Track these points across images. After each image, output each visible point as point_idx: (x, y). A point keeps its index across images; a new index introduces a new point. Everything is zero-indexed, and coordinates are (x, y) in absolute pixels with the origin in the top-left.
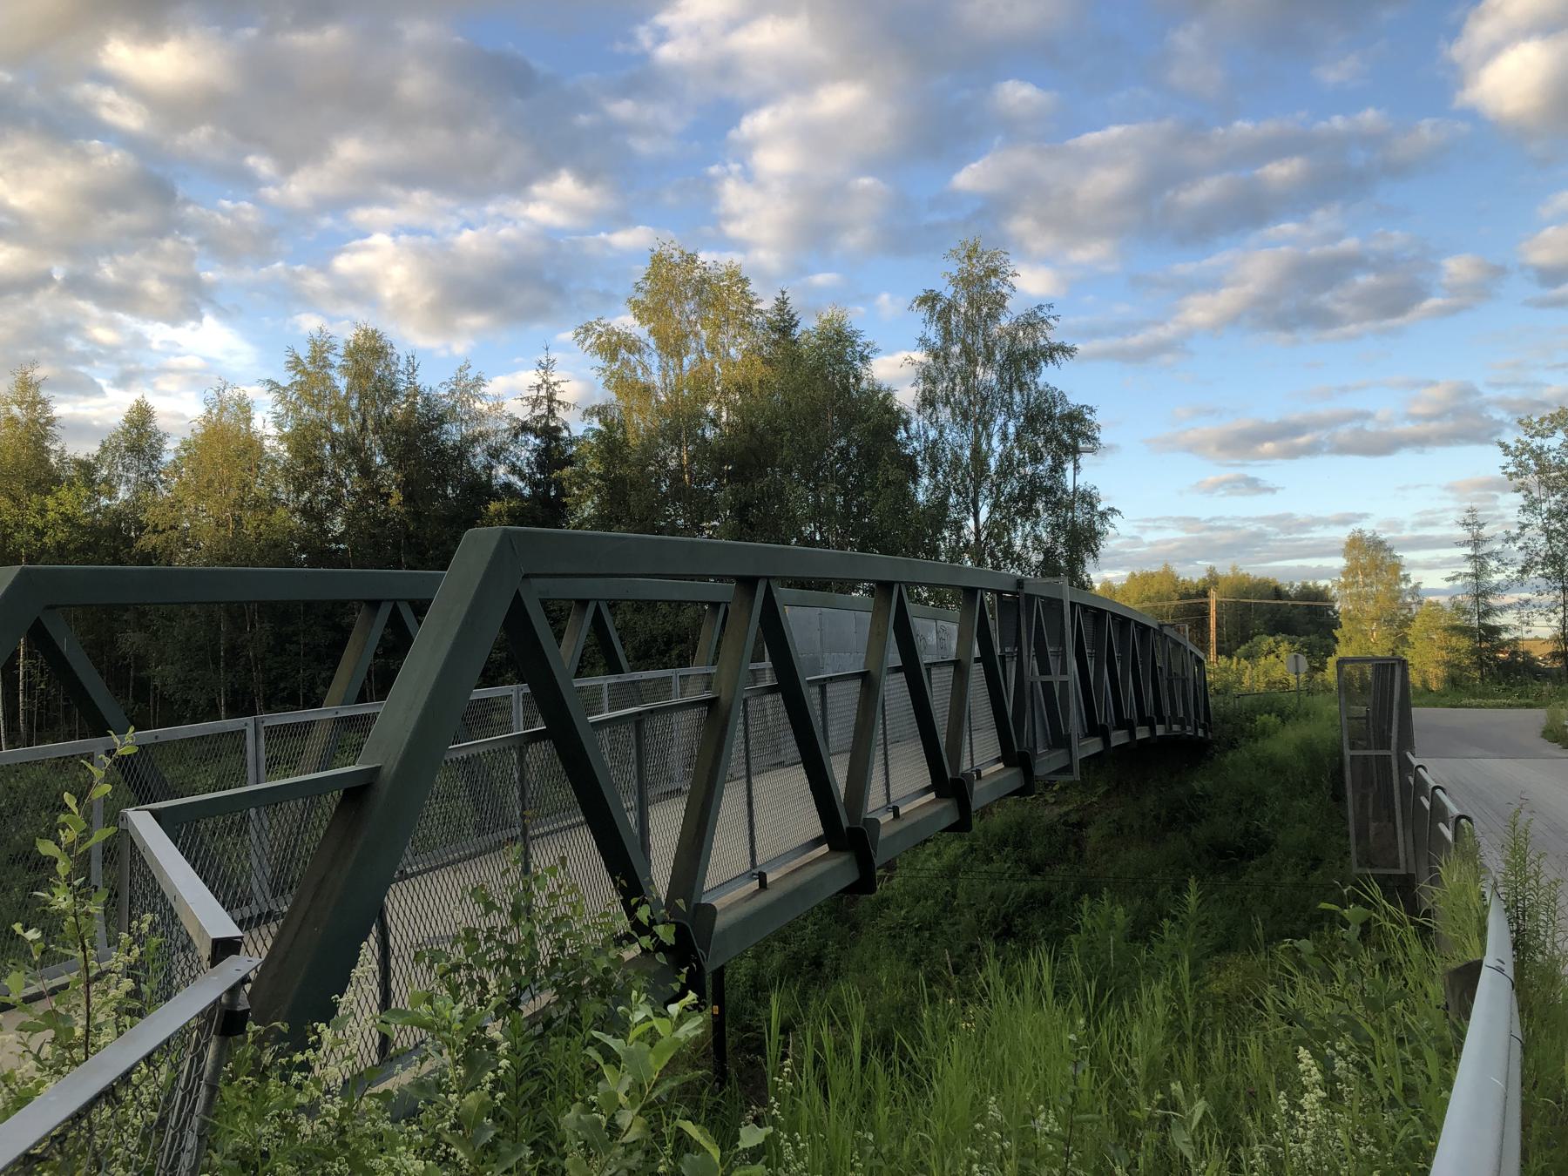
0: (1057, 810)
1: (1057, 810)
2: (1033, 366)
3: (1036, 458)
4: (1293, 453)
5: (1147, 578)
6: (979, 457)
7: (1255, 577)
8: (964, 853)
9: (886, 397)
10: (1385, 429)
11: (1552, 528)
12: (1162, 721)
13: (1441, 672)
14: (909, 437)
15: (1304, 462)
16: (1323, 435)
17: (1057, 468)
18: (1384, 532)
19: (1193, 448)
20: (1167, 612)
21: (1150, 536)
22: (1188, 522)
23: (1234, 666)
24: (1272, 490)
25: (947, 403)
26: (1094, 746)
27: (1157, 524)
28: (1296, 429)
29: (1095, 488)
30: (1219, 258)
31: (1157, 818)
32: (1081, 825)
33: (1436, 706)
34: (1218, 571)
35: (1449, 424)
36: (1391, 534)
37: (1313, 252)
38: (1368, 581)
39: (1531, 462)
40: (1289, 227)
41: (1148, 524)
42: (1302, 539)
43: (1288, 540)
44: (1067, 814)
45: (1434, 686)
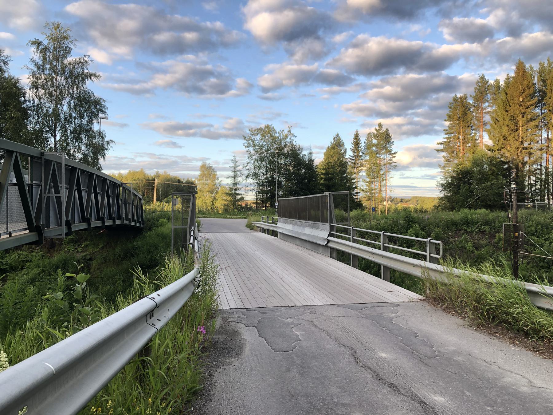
0: (82, 254)
1: (82, 254)
2: (83, 80)
3: (82, 117)
4: (188, 135)
5: (135, 173)
6: (56, 113)
7: (172, 175)
8: (40, 272)
9: (16, 83)
10: (216, 131)
11: (255, 164)
12: (119, 218)
13: (222, 207)
14: (25, 100)
15: (191, 139)
16: (198, 130)
17: (90, 122)
18: (214, 165)
19: (155, 129)
20: (141, 186)
21: (138, 159)
22: (152, 155)
23: (161, 205)
24: (181, 147)
25: (43, 88)
26: (84, 226)
27: (141, 155)
28: (189, 127)
29: (104, 131)
30: (168, 62)
31: (120, 256)
32: (91, 259)
33: (220, 218)
34: (159, 172)
35: (234, 132)
36: (216, 166)
37: (198, 67)
38: (206, 179)
39: (251, 143)
40: (191, 57)
41: (139, 155)
42: (188, 165)
43: (184, 164)
44: (85, 255)
45: (220, 211)
